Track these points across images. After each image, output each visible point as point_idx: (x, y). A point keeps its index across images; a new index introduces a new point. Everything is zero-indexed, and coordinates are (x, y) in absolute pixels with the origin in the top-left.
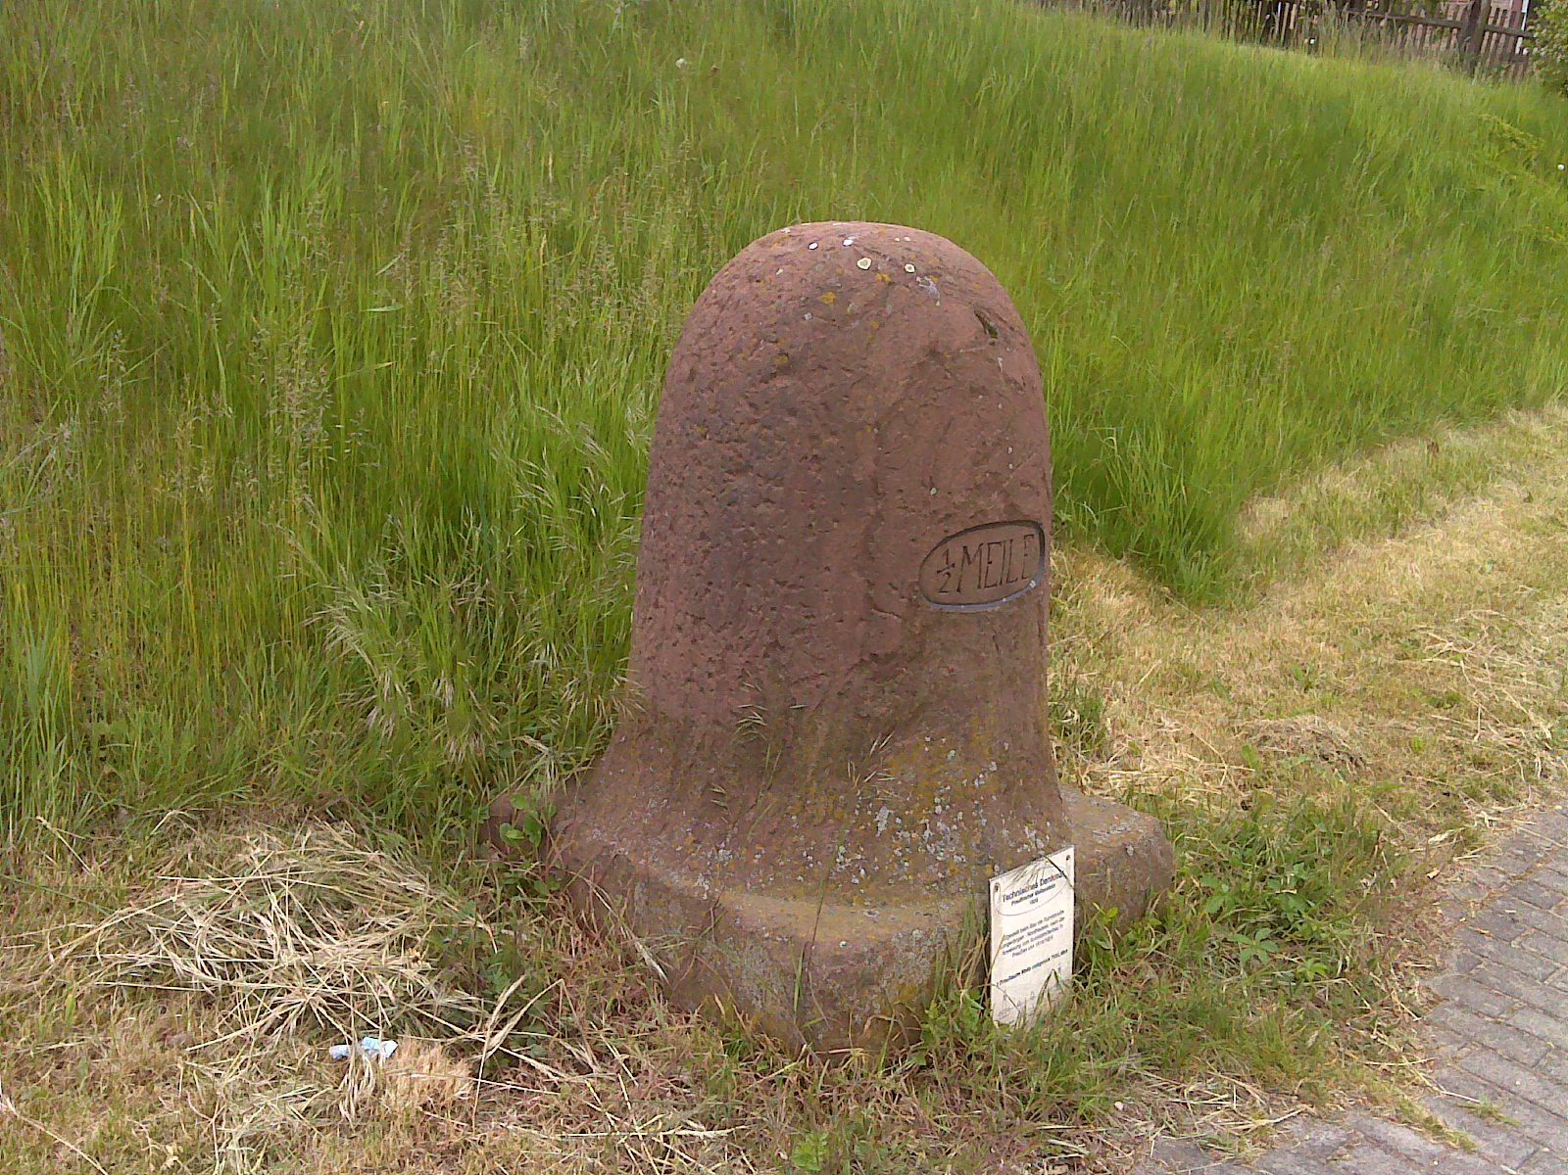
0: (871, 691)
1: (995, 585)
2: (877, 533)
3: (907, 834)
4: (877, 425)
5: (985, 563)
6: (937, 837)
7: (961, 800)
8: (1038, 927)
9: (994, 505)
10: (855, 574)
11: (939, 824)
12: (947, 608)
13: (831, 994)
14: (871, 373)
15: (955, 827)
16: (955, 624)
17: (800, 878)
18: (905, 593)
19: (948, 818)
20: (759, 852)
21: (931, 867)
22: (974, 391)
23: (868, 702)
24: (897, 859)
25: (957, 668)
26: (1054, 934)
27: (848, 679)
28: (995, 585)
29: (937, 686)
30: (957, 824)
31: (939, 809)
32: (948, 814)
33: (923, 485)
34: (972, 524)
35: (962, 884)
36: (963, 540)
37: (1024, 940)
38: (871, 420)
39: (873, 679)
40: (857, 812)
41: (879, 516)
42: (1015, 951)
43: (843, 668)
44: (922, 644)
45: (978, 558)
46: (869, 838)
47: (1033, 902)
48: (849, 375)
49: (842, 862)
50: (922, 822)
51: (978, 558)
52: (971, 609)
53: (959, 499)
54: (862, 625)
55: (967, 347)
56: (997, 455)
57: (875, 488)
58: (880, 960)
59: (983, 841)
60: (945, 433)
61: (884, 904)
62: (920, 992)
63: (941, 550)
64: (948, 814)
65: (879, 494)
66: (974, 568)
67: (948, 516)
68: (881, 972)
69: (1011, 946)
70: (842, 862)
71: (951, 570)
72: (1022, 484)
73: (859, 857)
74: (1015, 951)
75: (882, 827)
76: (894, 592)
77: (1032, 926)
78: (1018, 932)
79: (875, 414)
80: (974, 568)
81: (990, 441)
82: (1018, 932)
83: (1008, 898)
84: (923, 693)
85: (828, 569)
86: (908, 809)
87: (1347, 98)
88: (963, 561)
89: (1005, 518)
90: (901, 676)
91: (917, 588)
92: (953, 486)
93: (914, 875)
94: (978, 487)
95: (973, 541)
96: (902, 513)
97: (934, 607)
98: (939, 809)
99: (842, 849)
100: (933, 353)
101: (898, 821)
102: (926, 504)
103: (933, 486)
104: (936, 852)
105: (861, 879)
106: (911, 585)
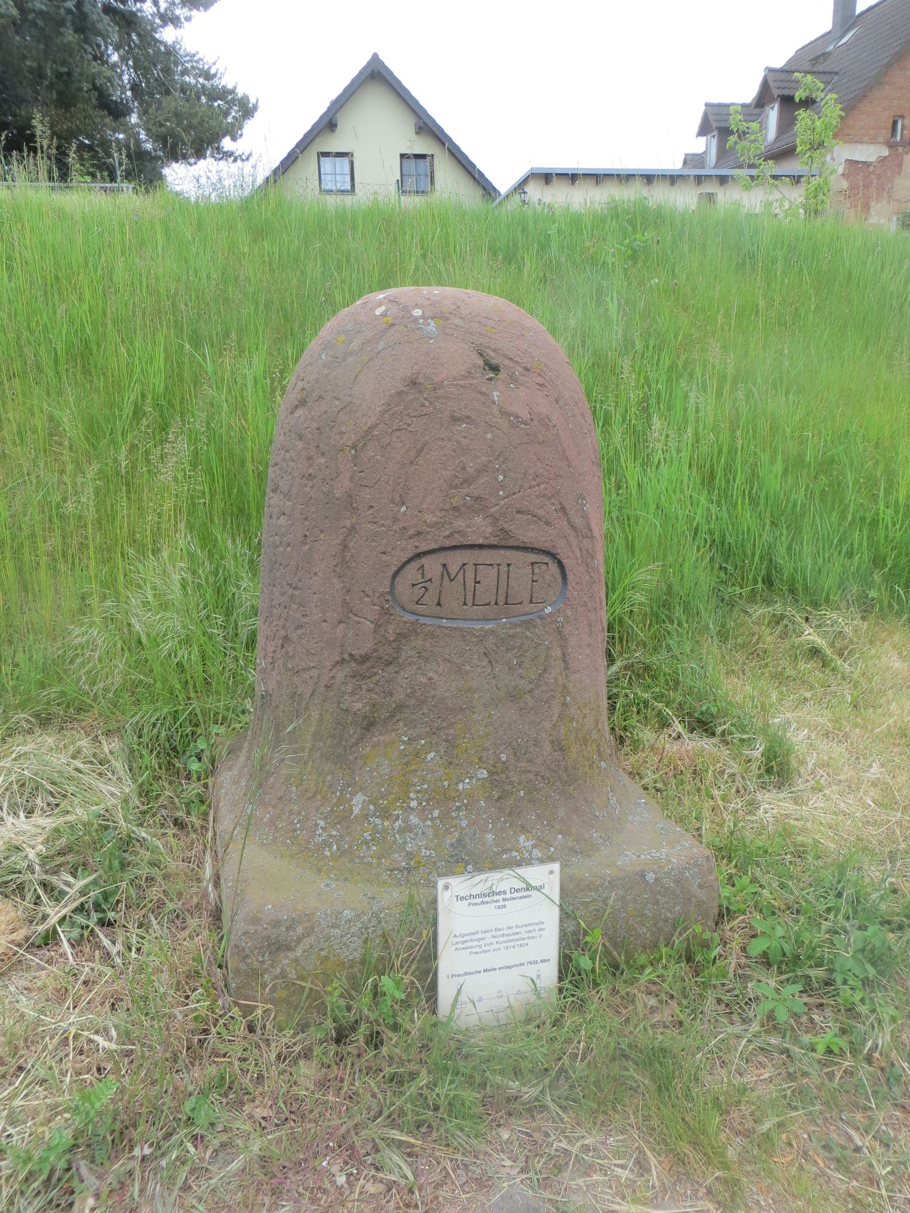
0: (349, 688)
1: (488, 604)
2: (351, 544)
3: (378, 821)
4: (354, 447)
5: (470, 583)
6: (408, 828)
7: (442, 798)
8: (506, 932)
9: (479, 528)
10: (335, 580)
11: (411, 817)
12: (423, 620)
13: (243, 950)
14: (354, 400)
15: (429, 823)
16: (432, 635)
17: (288, 841)
18: (376, 601)
19: (422, 812)
20: (269, 813)
21: (396, 855)
22: (455, 419)
23: (347, 697)
24: (366, 842)
25: (436, 677)
26: (530, 942)
27: (332, 674)
28: (488, 604)
29: (414, 692)
30: (432, 819)
31: (414, 804)
32: (424, 809)
33: (392, 501)
34: (448, 543)
35: (426, 876)
36: (442, 558)
37: (487, 941)
38: (350, 443)
39: (354, 677)
40: (338, 794)
41: (353, 528)
42: (474, 950)
43: (328, 663)
44: (398, 650)
45: (460, 577)
46: (343, 818)
47: (499, 907)
48: (337, 403)
49: (321, 836)
50: (395, 813)
51: (460, 577)
52: (454, 624)
53: (430, 518)
54: (342, 626)
55: (455, 379)
56: (482, 481)
57: (350, 503)
58: (300, 930)
59: (459, 841)
60: (418, 455)
61: (346, 879)
62: (352, 967)
63: (415, 565)
64: (424, 809)
65: (354, 509)
66: (457, 585)
67: (419, 533)
68: (299, 941)
69: (466, 945)
70: (321, 836)
71: (427, 584)
72: (519, 512)
73: (334, 833)
74: (474, 950)
75: (356, 810)
76: (367, 599)
77: (497, 930)
78: (477, 933)
79: (353, 437)
80: (457, 585)
81: (471, 467)
82: (477, 933)
83: (462, 898)
84: (400, 696)
85: (315, 574)
86: (382, 798)
87: (393, 210)
88: (442, 575)
89: (493, 541)
90: (378, 677)
91: (389, 598)
92: (425, 506)
93: (379, 859)
94: (456, 509)
95: (455, 560)
96: (371, 527)
97: (408, 617)
98: (414, 804)
99: (322, 823)
100: (414, 383)
101: (372, 807)
102: (395, 520)
103: (403, 503)
104: (405, 843)
105: (332, 854)
106: (382, 595)
